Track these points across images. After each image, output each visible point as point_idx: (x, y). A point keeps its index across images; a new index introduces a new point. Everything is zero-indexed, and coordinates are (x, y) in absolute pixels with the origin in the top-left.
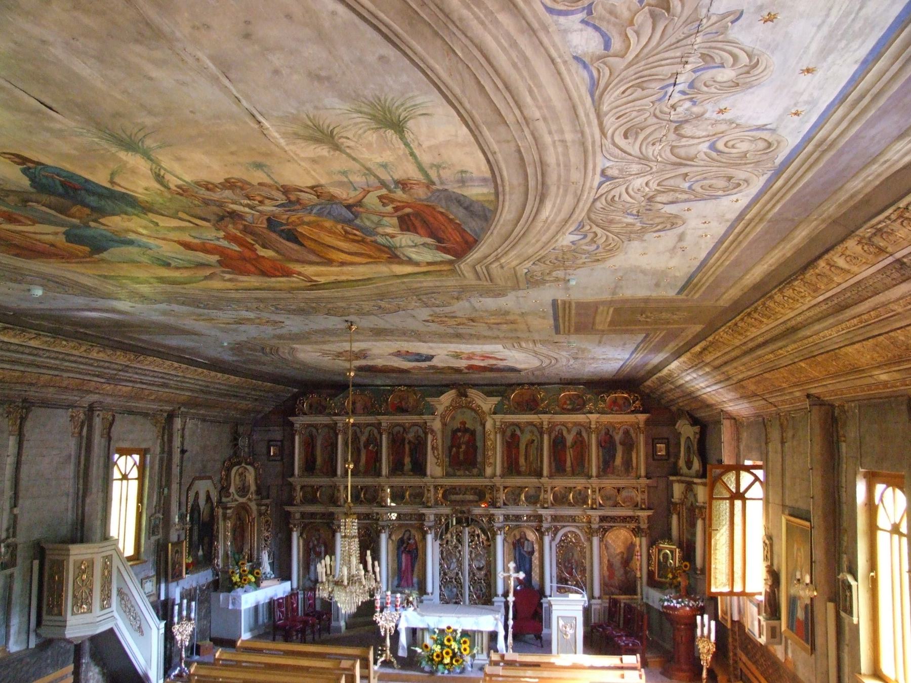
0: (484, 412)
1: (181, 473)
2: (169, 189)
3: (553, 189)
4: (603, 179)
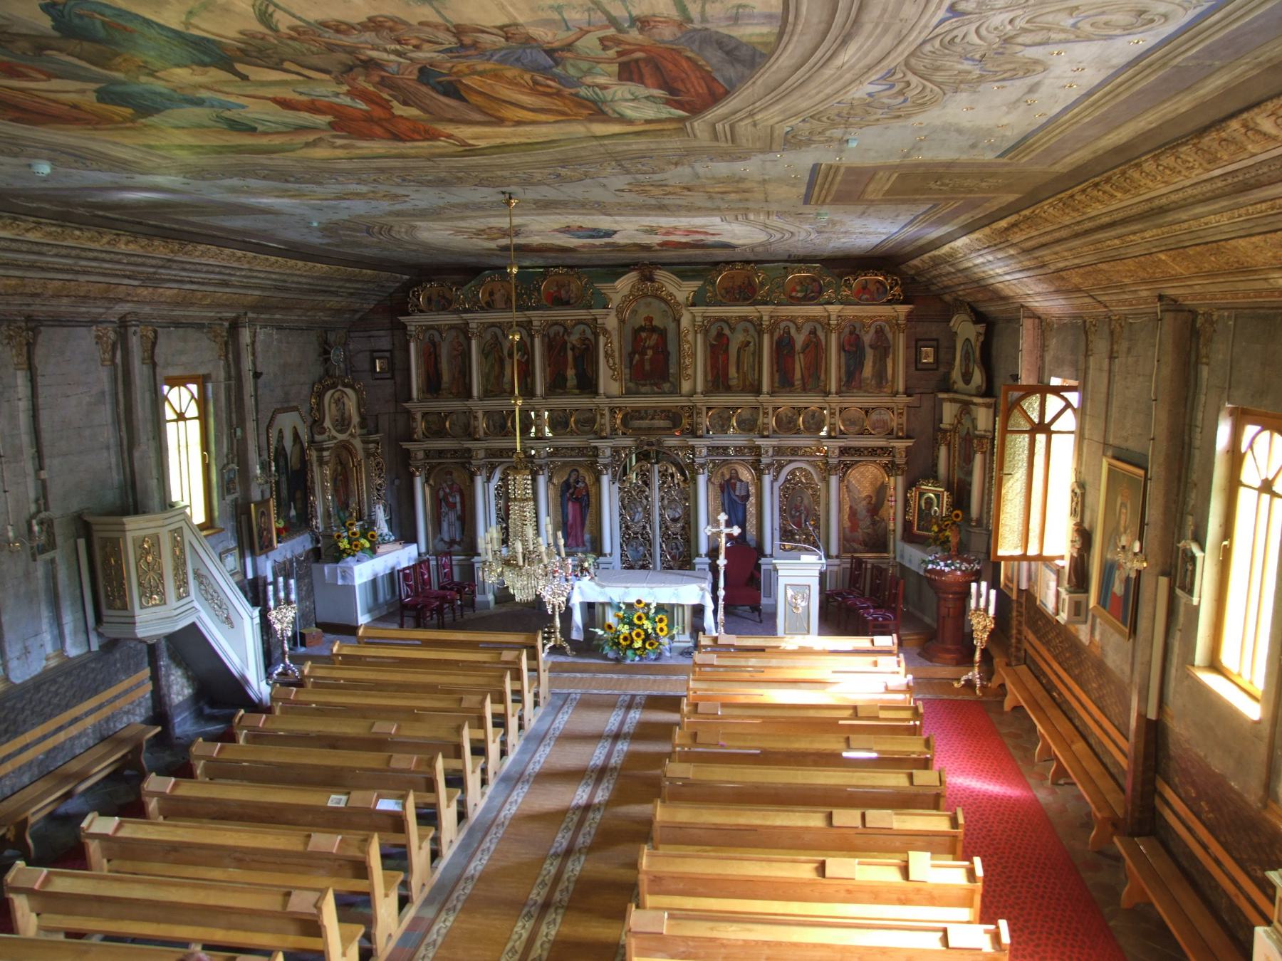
0: (678, 304)
1: (257, 405)
2: (276, 30)
3: (868, 27)
4: (949, 15)
